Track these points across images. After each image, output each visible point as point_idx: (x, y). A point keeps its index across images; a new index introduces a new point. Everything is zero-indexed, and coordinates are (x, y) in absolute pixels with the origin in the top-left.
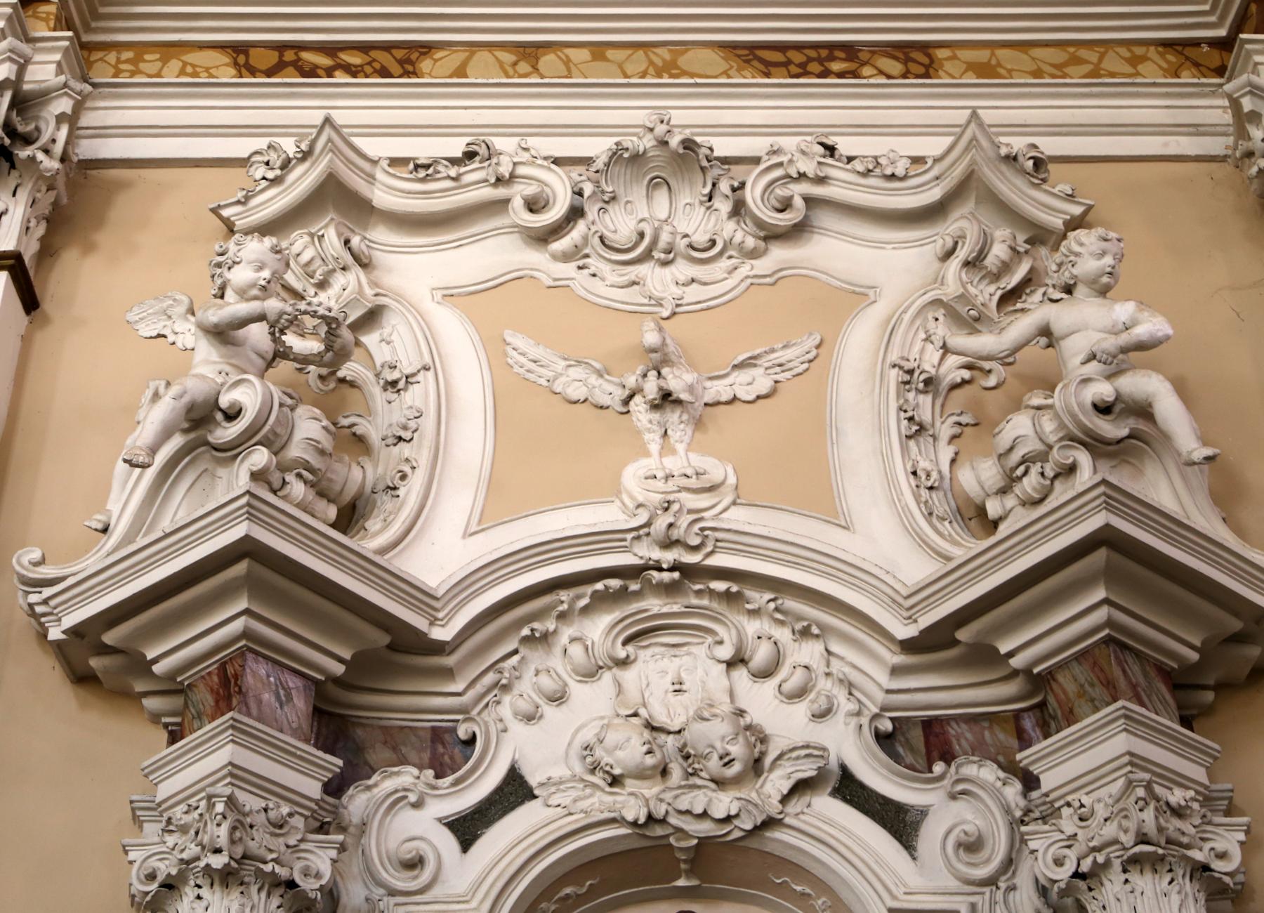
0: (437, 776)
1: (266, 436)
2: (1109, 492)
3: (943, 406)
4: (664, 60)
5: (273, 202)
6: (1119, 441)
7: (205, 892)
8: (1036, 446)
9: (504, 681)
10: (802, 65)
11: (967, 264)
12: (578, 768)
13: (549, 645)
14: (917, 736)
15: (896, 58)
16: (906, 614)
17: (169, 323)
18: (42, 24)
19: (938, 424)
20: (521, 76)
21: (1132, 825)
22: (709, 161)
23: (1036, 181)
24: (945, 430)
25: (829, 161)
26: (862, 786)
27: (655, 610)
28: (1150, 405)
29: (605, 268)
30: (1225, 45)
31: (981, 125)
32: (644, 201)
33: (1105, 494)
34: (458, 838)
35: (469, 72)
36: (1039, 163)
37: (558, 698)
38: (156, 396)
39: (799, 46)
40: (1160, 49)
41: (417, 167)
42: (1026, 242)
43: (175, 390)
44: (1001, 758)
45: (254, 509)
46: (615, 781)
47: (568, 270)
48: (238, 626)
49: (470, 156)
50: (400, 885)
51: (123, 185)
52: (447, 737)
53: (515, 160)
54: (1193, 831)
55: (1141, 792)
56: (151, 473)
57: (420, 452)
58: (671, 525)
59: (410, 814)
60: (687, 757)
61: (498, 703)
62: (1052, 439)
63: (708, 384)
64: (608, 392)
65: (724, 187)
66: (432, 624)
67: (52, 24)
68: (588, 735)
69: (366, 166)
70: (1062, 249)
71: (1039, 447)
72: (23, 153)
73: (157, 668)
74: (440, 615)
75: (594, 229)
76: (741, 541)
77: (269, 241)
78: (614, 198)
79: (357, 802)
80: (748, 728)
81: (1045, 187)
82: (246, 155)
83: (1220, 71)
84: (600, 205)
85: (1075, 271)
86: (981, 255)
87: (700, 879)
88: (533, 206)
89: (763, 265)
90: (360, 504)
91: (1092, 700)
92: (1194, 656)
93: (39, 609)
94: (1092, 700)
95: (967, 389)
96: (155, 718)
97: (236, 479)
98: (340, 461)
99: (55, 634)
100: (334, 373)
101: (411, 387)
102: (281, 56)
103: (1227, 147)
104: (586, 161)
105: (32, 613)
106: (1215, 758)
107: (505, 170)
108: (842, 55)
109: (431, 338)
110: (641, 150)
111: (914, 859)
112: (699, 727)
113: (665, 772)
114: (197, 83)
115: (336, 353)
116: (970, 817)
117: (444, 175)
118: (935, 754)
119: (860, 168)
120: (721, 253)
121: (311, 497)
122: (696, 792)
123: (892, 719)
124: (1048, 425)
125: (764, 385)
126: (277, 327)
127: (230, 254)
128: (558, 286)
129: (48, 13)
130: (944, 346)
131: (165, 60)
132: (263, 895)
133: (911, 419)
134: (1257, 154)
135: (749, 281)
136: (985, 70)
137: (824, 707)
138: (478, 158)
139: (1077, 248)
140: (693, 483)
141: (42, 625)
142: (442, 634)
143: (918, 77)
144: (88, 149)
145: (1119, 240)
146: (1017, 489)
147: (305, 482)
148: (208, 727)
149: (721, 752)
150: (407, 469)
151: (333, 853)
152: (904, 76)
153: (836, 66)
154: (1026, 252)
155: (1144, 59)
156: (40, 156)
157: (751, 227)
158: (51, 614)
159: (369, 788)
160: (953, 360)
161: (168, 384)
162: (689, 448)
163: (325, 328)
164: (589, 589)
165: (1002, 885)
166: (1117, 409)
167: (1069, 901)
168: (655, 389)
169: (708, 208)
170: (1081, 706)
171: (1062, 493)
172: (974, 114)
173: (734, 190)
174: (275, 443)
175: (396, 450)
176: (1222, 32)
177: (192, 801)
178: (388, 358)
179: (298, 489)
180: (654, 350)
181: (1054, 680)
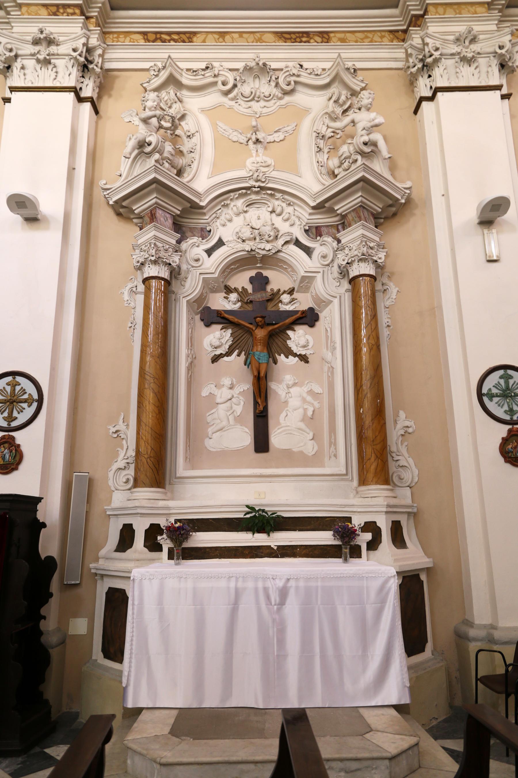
0: (202, 240)
1: (158, 150)
2: (365, 167)
3: (326, 143)
4: (258, 37)
5: (157, 82)
6: (368, 153)
7: (150, 265)
8: (348, 154)
9: (218, 216)
10: (295, 39)
11: (335, 102)
12: (235, 238)
13: (228, 207)
14: (314, 230)
15: (319, 37)
16: (313, 199)
17: (132, 118)
18: (92, 25)
19: (324, 148)
20: (220, 42)
21: (361, 251)
22: (270, 70)
23: (354, 76)
24: (326, 150)
25: (301, 70)
26: (301, 243)
27: (254, 198)
28: (377, 143)
29: (242, 103)
30: (405, 31)
31: (341, 58)
32: (253, 82)
33: (364, 167)
34: (207, 254)
35: (206, 41)
36: (355, 70)
37: (230, 221)
38: (130, 139)
39: (294, 33)
40: (389, 33)
41: (194, 71)
42: (350, 95)
43: (135, 137)
44: (333, 236)
45: (156, 170)
46: (244, 241)
47: (233, 103)
48: (154, 201)
49: (207, 68)
50: (194, 265)
51: (117, 77)
52: (205, 230)
53: (219, 69)
54: (374, 253)
55: (364, 243)
56: (131, 160)
57: (196, 155)
58: (258, 176)
59: (196, 248)
60: (260, 235)
61: (216, 221)
62: (352, 152)
63: (268, 137)
64: (243, 139)
65: (273, 78)
66: (200, 201)
67: (94, 25)
68: (237, 230)
69: (180, 71)
70: (359, 97)
71: (349, 154)
72: (91, 66)
73: (136, 212)
74: (202, 199)
75: (239, 91)
76: (275, 180)
77: (156, 93)
78: (245, 81)
79: (184, 246)
80: (275, 228)
81: (356, 78)
82: (148, 68)
83: (403, 40)
84: (242, 83)
85: (362, 103)
86: (339, 99)
87: (262, 264)
88: (224, 84)
89: (283, 102)
90: (182, 170)
91: (355, 221)
92: (380, 210)
93: (107, 196)
94: (355, 221)
95: (332, 139)
96: (136, 224)
97: (151, 162)
98: (177, 158)
99: (111, 203)
100: (174, 133)
101: (194, 137)
102: (156, 36)
103: (403, 65)
104: (237, 70)
105: (105, 198)
106: (382, 235)
107: (216, 73)
108: (305, 35)
109: (198, 123)
110: (252, 66)
111: (311, 260)
112: (263, 228)
113: (255, 239)
114: (134, 46)
115: (175, 126)
116: (324, 250)
117: (200, 74)
118: (318, 235)
119: (309, 72)
120: (272, 98)
121: (264, 295)
122: (262, 244)
123: (308, 226)
124: (352, 148)
125: (282, 137)
126: (160, 119)
127: (146, 97)
128: (231, 108)
129: (93, 22)
130: (327, 126)
131: (125, 37)
132: (164, 266)
133: (318, 147)
134: (411, 67)
135: (279, 107)
136: (343, 40)
137: (293, 223)
138: (209, 69)
139: (363, 96)
140: (264, 164)
141: (108, 200)
142: (202, 204)
143: (325, 43)
144: (108, 66)
145: (374, 94)
146: (343, 167)
147: (168, 163)
148: (149, 226)
149: (268, 234)
150: (193, 160)
151: (179, 257)
152: (322, 43)
153: (304, 39)
154: (350, 98)
155: (384, 36)
156: (95, 67)
157: (280, 91)
158: (109, 197)
159: (186, 242)
160: (330, 130)
161: (133, 135)
162: (263, 155)
163: (171, 120)
164: (238, 193)
165: (330, 266)
166: (369, 144)
167: (345, 269)
168: (255, 138)
169: (269, 84)
170: (353, 223)
171: (353, 167)
172: (339, 55)
173: (276, 79)
174: (161, 152)
175: (190, 155)
176: (405, 27)
177: (146, 244)
178: (188, 129)
179: (167, 165)
180: (254, 127)
181: (347, 216)
